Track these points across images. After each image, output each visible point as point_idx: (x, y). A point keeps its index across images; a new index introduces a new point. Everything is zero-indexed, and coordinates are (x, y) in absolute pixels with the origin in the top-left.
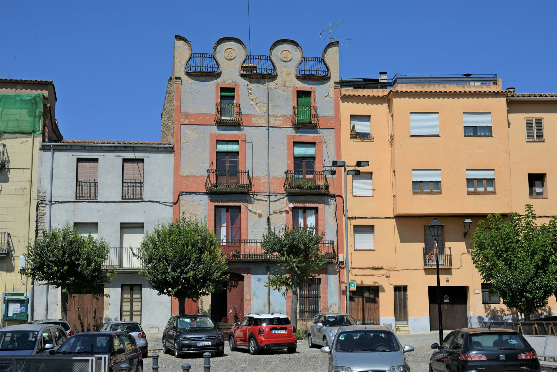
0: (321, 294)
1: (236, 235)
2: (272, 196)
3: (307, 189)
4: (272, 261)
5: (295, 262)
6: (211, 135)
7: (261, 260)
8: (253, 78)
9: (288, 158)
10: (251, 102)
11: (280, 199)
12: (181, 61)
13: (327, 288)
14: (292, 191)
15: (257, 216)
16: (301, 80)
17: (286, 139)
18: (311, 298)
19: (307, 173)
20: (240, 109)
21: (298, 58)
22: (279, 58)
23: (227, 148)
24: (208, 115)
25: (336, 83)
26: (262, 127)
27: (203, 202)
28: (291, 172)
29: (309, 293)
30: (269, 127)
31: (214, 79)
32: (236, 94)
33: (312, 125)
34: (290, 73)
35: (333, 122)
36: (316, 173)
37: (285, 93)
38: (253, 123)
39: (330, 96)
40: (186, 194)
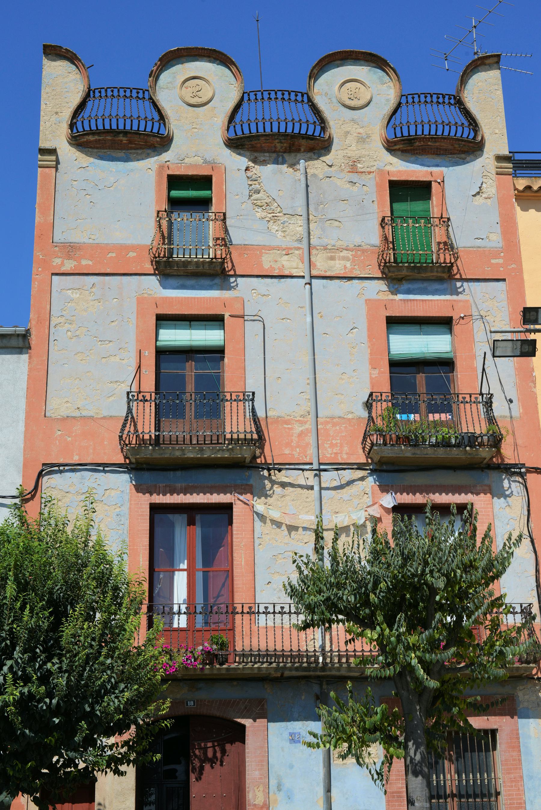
0: (500, 781)
1: (218, 597)
2: (325, 470)
3: (437, 445)
4: (334, 673)
5: (415, 648)
6: (140, 301)
7: (297, 669)
8: (262, 150)
9: (371, 364)
10: (260, 213)
11: (354, 481)
12: (58, 110)
13: (520, 760)
14: (389, 452)
15: (286, 532)
16: (399, 153)
17: (363, 310)
18: (468, 796)
19: (433, 409)
20: (226, 231)
21: (388, 100)
22: (334, 100)
23: (188, 338)
24: (133, 248)
25: (500, 158)
26: (292, 277)
27: (113, 493)
28: (384, 398)
29: (460, 781)
30: (312, 277)
31: (153, 154)
32: (215, 194)
33: (440, 266)
34: (369, 137)
35: (501, 261)
36: (461, 399)
37: (355, 189)
38: (266, 266)
39: (484, 196)
40: (61, 472)
